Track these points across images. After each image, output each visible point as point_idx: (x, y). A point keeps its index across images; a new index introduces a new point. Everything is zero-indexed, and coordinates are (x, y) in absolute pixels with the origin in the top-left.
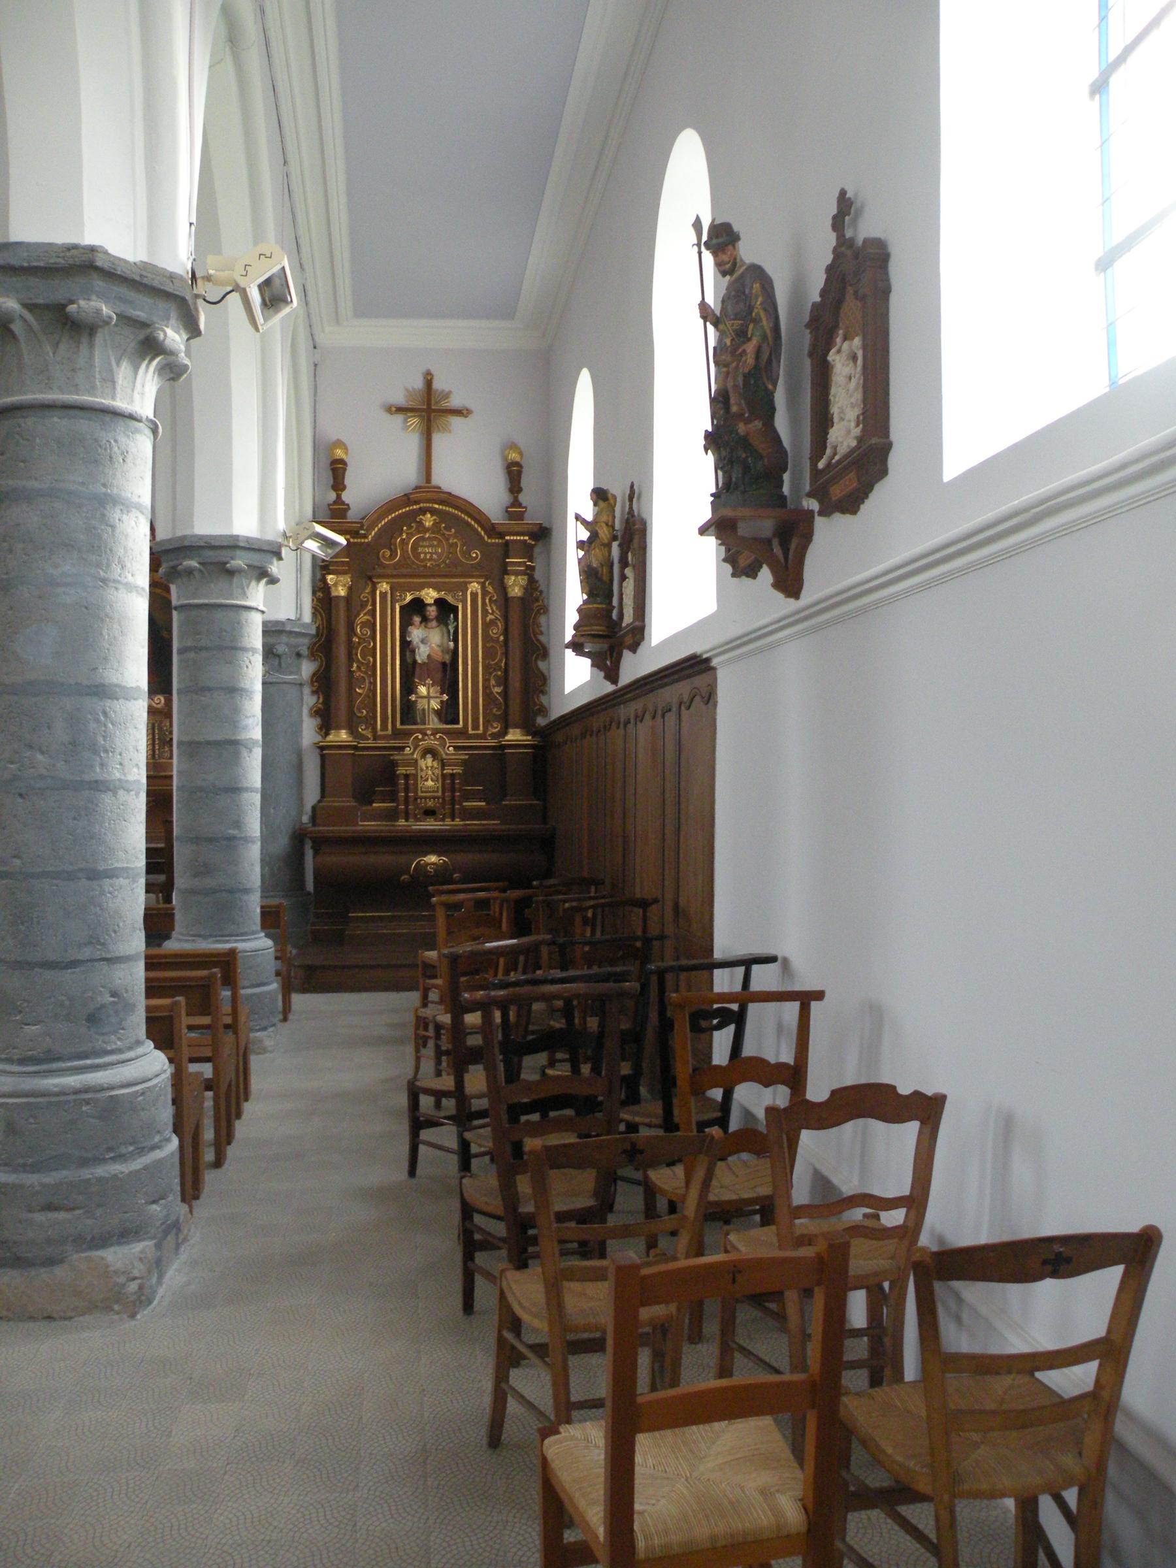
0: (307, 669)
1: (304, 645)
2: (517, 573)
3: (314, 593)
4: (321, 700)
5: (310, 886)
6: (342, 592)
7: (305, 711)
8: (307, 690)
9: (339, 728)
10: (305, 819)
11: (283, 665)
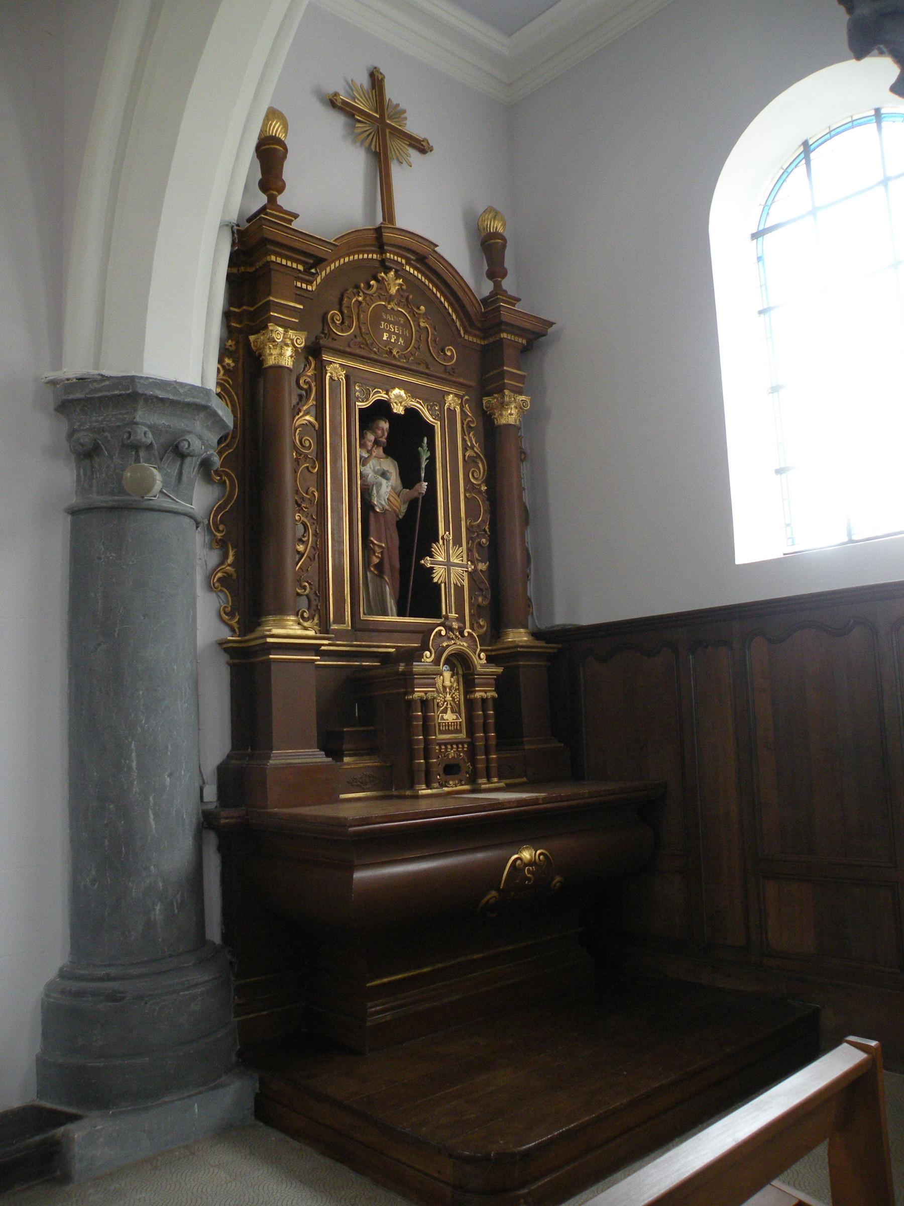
0: (201, 498)
1: (202, 440)
2: (286, 326)
3: (220, 361)
4: (230, 559)
5: (214, 932)
6: (287, 358)
7: (199, 578)
8: (199, 539)
9: (281, 610)
10: (211, 793)
11: (185, 478)
